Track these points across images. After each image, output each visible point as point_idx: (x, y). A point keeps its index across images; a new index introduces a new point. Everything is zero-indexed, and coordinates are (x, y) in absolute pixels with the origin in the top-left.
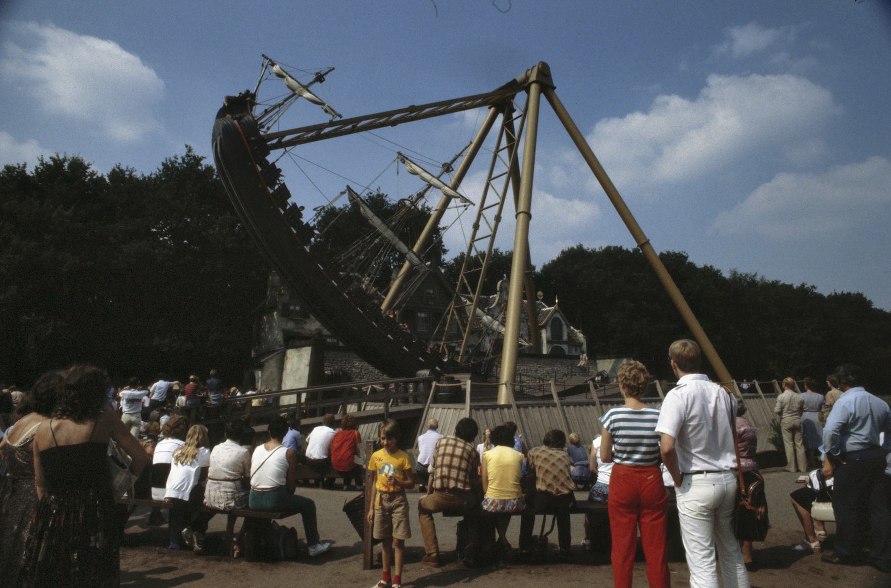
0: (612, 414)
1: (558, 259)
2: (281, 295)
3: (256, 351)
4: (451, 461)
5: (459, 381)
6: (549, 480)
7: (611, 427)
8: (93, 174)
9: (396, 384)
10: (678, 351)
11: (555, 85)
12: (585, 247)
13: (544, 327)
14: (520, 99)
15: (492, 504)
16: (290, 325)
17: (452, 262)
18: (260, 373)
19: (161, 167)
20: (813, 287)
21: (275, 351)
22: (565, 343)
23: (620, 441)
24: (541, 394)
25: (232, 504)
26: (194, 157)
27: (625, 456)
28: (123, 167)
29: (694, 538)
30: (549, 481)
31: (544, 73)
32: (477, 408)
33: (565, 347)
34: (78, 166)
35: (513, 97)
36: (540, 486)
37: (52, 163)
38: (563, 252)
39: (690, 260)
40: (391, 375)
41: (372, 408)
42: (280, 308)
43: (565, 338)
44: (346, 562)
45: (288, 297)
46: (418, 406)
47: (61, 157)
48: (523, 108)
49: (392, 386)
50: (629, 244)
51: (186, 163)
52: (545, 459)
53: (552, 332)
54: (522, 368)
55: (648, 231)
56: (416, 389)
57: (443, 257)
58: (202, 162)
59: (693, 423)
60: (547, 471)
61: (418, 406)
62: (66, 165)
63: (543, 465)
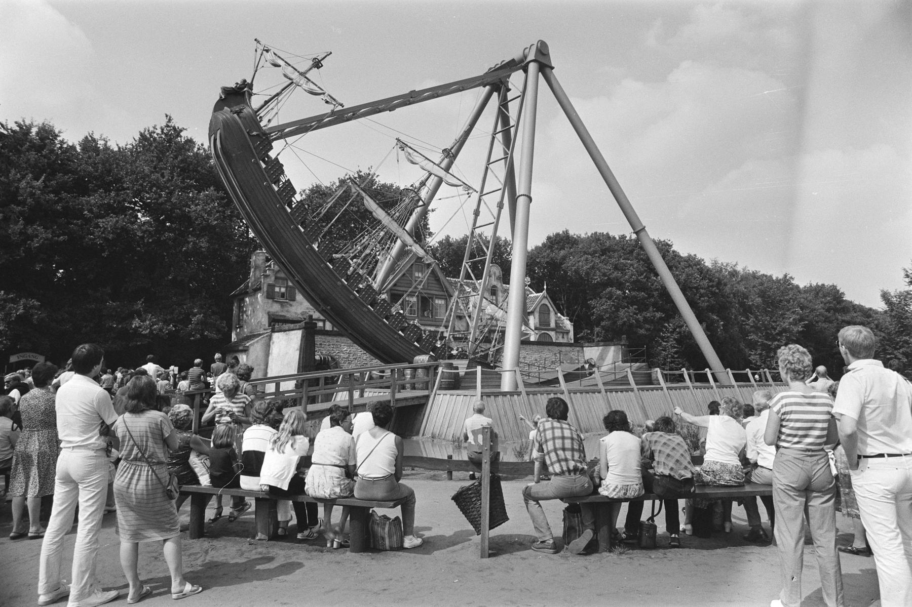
0: (782, 398)
1: (544, 244)
2: (266, 276)
3: (237, 334)
4: (563, 444)
5: (457, 368)
6: (671, 464)
7: (783, 411)
8: (62, 142)
9: (392, 371)
10: (852, 338)
11: (553, 65)
12: (571, 233)
13: (532, 313)
14: (516, 80)
15: (614, 490)
16: (276, 308)
17: (437, 245)
18: (244, 357)
19: (137, 137)
20: (791, 278)
21: (260, 335)
22: (552, 330)
23: (792, 424)
24: (537, 380)
25: (338, 490)
26: (174, 128)
27: (796, 440)
28: (96, 136)
29: (878, 521)
30: (671, 465)
31: (542, 51)
32: (488, 395)
33: (552, 334)
34: (47, 134)
35: (509, 76)
36: (661, 470)
37: (18, 129)
38: (549, 238)
39: (674, 248)
40: (386, 362)
41: (371, 395)
42: (265, 289)
43: (553, 325)
44: (454, 551)
45: (273, 278)
46: (426, 393)
47: (28, 122)
48: (521, 88)
49: (388, 373)
50: (619, 229)
51: (166, 135)
52: (665, 444)
53: (540, 319)
54: (523, 353)
55: (645, 220)
56: (413, 376)
57: (429, 239)
58: (182, 134)
59: (872, 406)
60: (668, 455)
61: (426, 393)
62: (34, 130)
63: (662, 449)
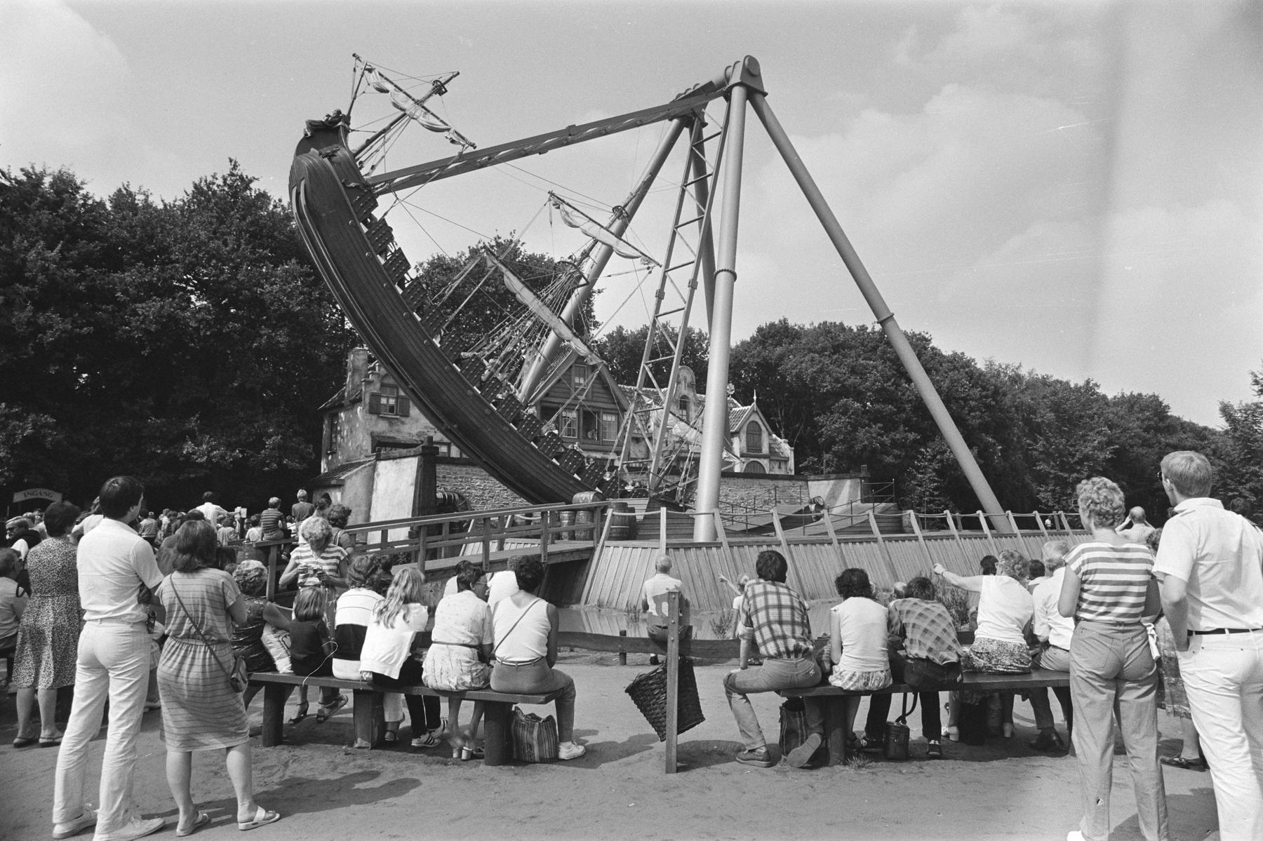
0: (1083, 551)
1: (753, 339)
2: (369, 383)
3: (328, 463)
4: (780, 615)
5: (632, 510)
6: (929, 643)
7: (1084, 569)
8: (86, 197)
9: (543, 514)
11: (766, 90)
12: (791, 323)
13: (737, 433)
14: (714, 110)
15: (851, 679)
16: (382, 427)
17: (605, 339)
18: (339, 494)
19: (190, 190)
20: (1096, 385)
21: (360, 464)
22: (765, 457)
23: (1096, 588)
24: (743, 527)
25: (468, 679)
26: (241, 178)
27: (1102, 609)
28: (133, 189)
29: (1216, 722)
30: (929, 644)
31: (751, 70)
32: (676, 548)
33: (765, 462)
34: (65, 186)
35: (705, 106)
36: (915, 651)
37: (24, 178)
38: (760, 330)
39: (934, 344)
40: (535, 501)
41: (513, 547)
42: (367, 400)
43: (765, 450)
44: (629, 764)
45: (378, 385)
46: (589, 544)
47: (38, 170)
48: (722, 122)
49: (537, 517)
50: (857, 317)
51: (230, 187)
52: (921, 615)
53: (748, 442)
54: (725, 489)
55: (893, 305)
56: (573, 521)
57: (593, 332)
58: (252, 185)
59: (1207, 563)
60: (926, 631)
61: (589, 544)
62: (47, 181)
63: (917, 622)
